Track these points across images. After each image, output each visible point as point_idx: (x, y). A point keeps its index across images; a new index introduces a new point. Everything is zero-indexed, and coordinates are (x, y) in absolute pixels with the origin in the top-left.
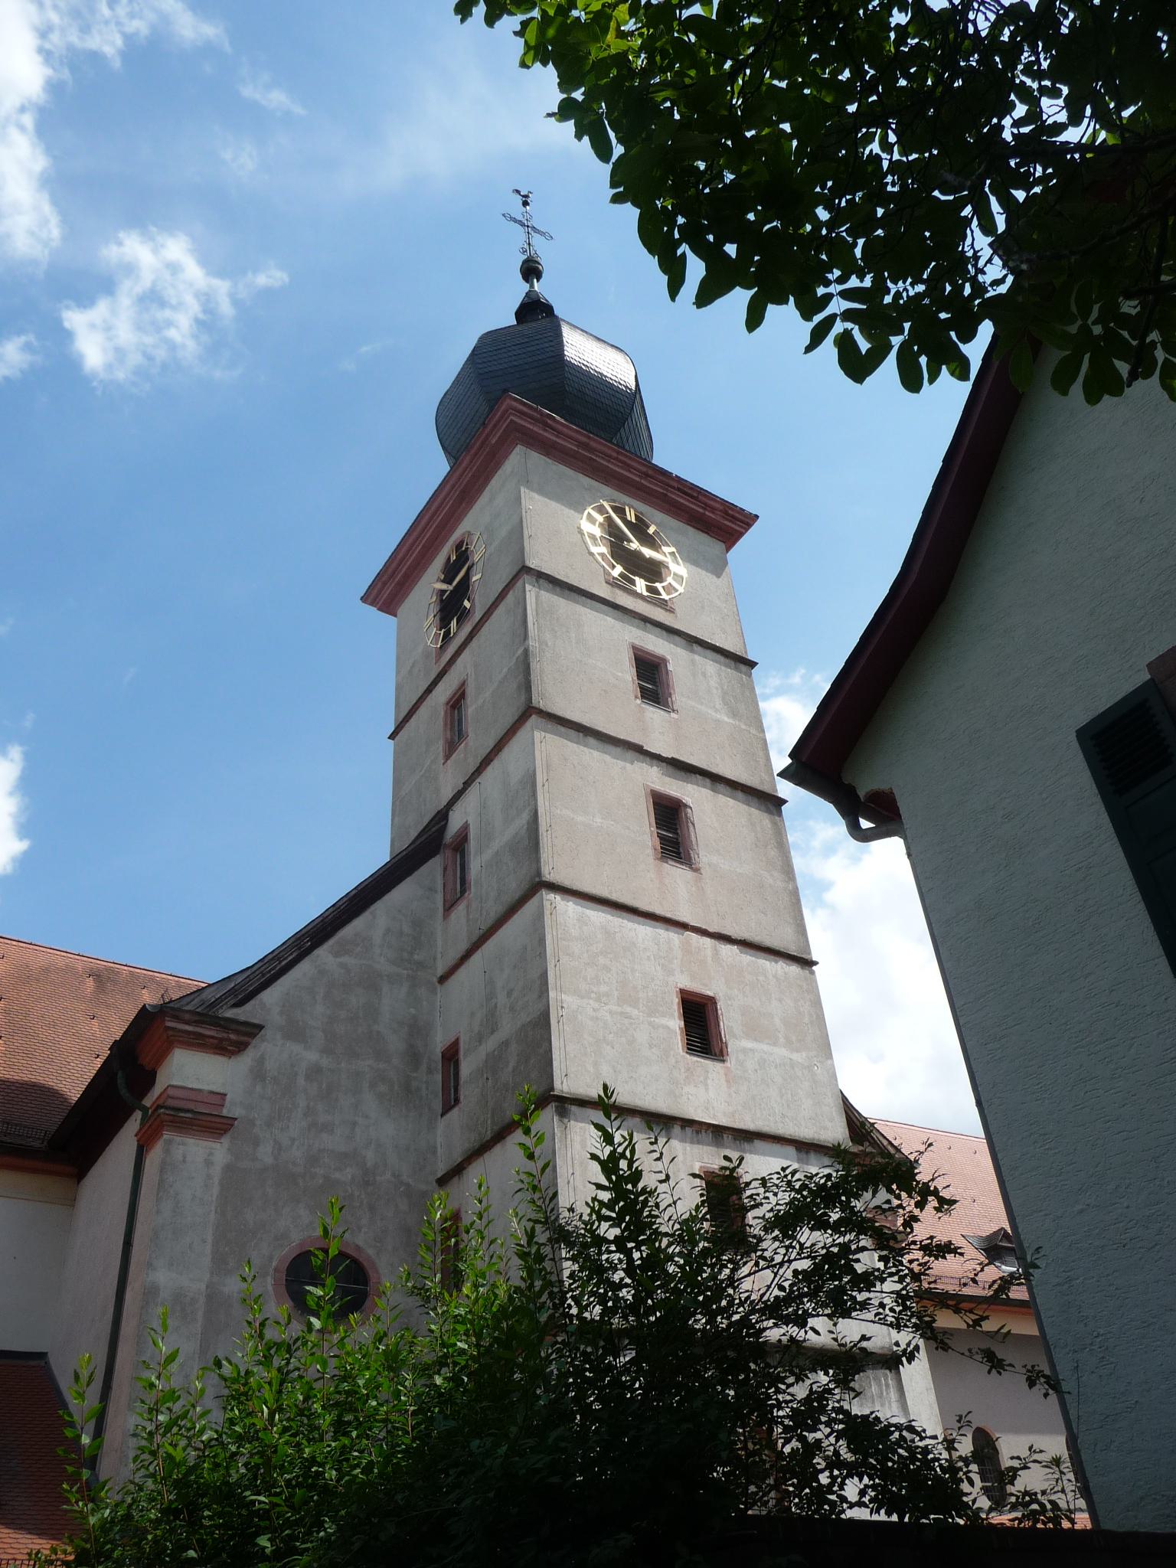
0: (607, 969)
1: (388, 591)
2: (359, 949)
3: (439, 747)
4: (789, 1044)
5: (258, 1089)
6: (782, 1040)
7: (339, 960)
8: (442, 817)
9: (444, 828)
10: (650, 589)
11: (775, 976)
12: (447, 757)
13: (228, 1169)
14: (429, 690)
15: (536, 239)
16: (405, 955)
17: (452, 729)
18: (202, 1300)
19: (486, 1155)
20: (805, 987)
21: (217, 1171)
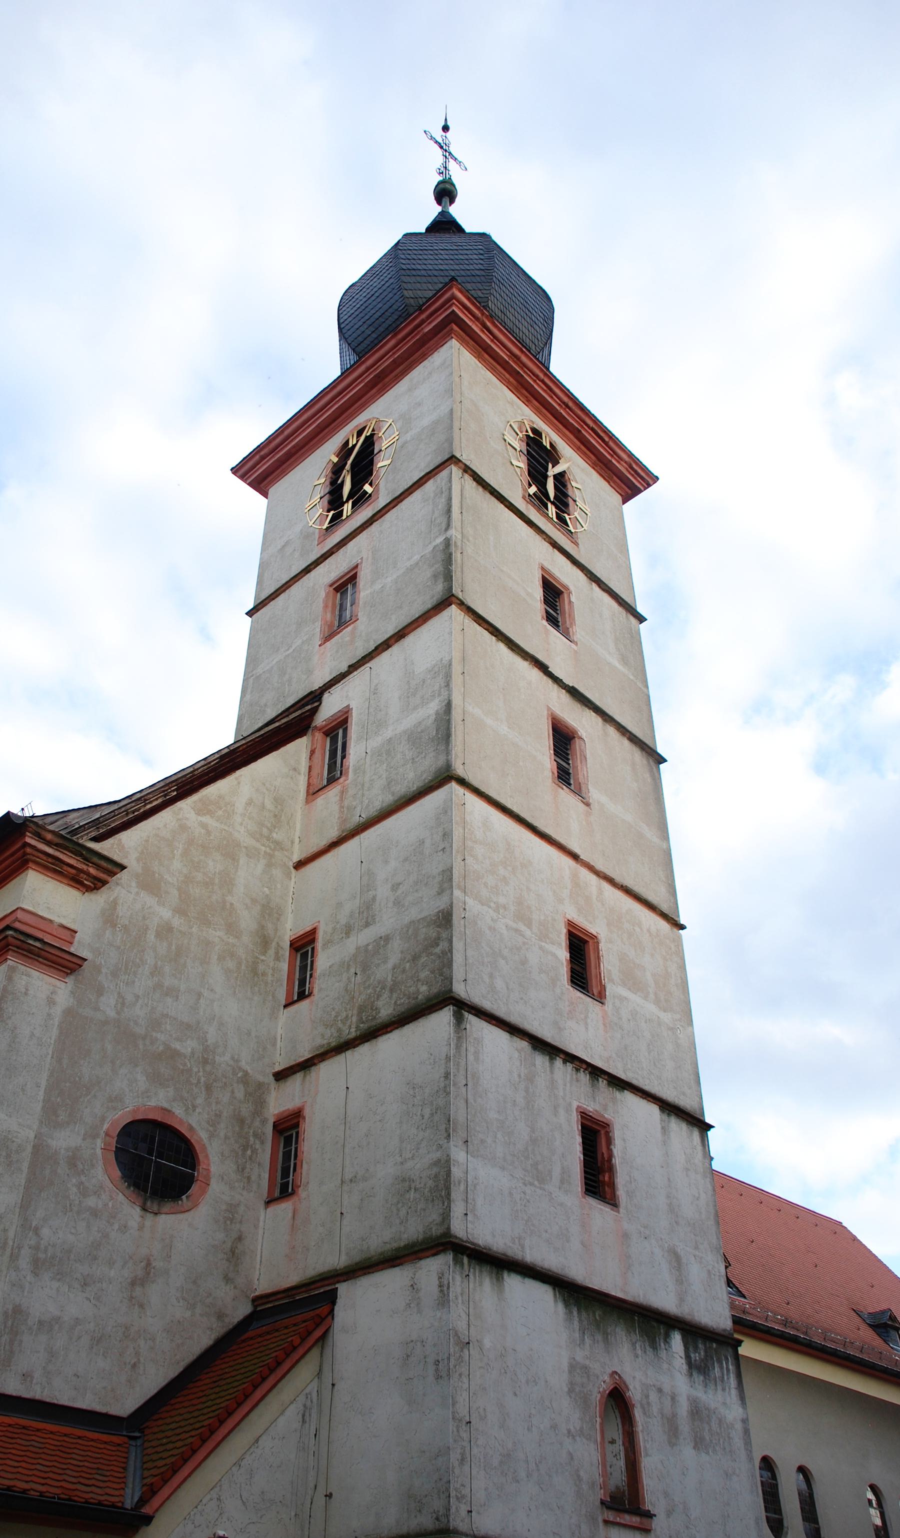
0: (505, 880)
1: (262, 469)
2: (220, 813)
3: (316, 630)
4: (657, 1002)
5: (108, 933)
6: (652, 996)
7: (200, 818)
8: (315, 697)
9: (315, 711)
10: (558, 517)
11: (649, 931)
12: (327, 638)
13: (69, 1012)
14: (307, 570)
15: (452, 164)
16: (265, 831)
17: (333, 612)
18: (29, 1149)
19: (349, 1053)
20: (673, 949)
21: (57, 1011)
